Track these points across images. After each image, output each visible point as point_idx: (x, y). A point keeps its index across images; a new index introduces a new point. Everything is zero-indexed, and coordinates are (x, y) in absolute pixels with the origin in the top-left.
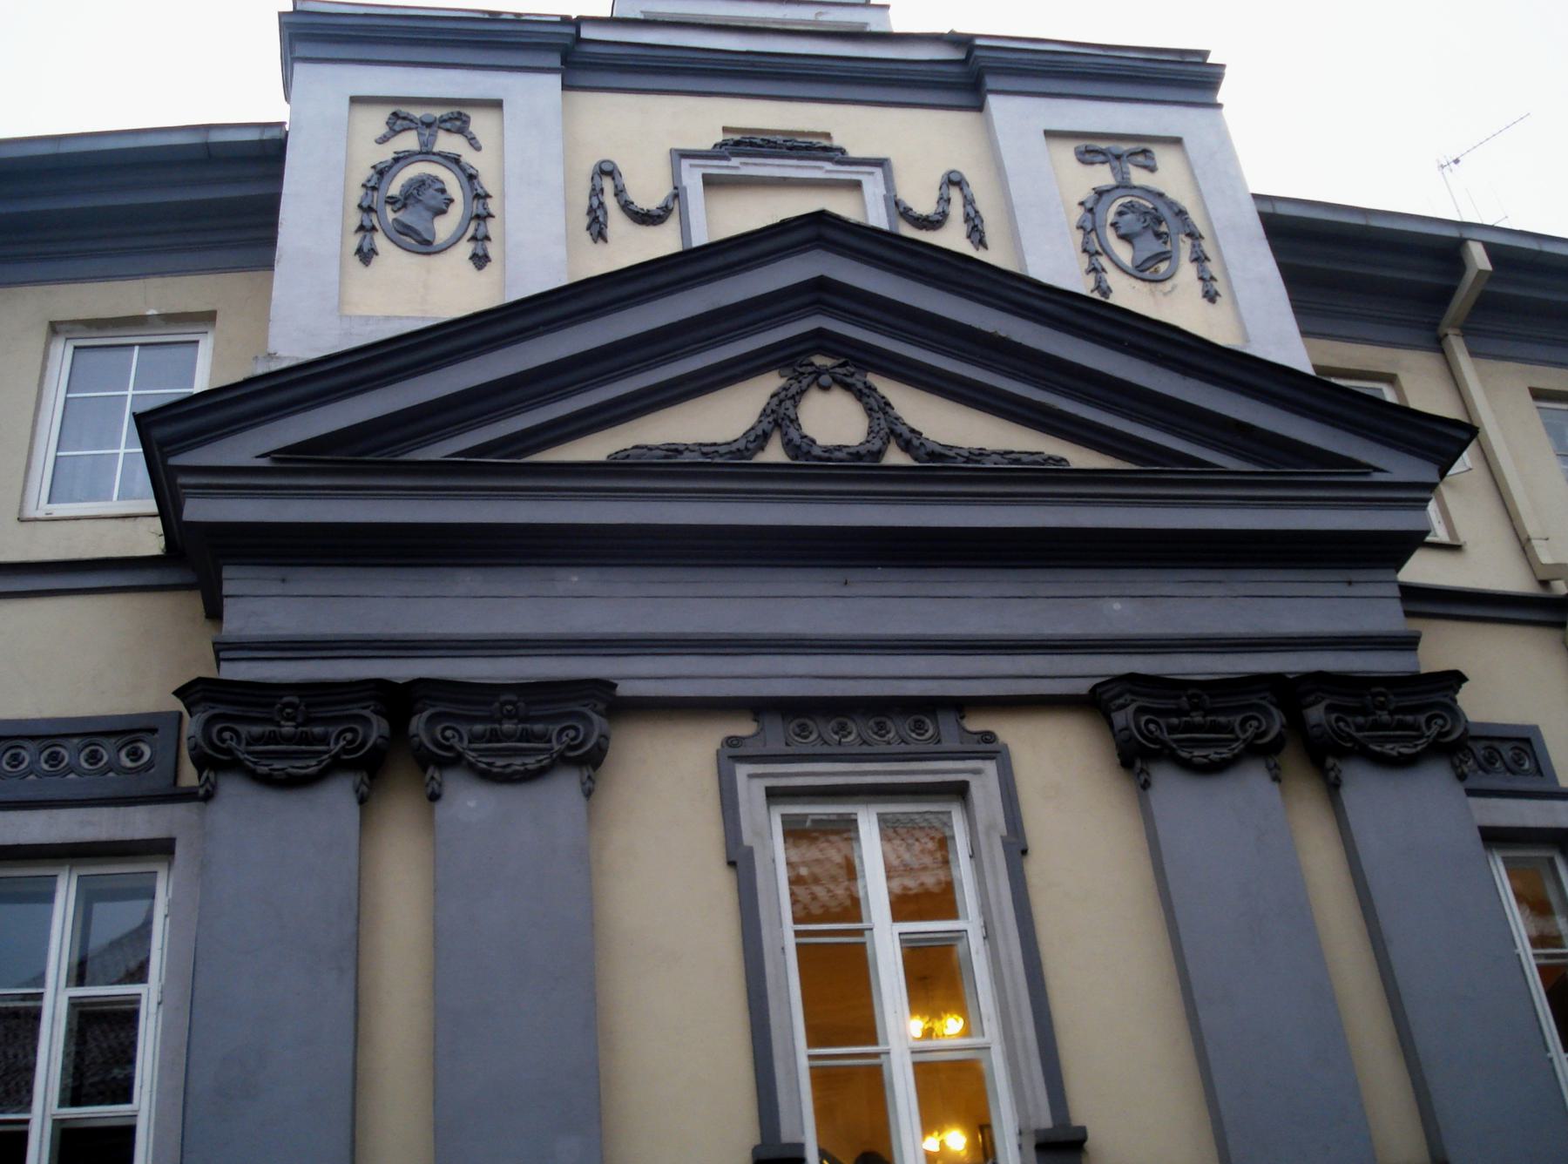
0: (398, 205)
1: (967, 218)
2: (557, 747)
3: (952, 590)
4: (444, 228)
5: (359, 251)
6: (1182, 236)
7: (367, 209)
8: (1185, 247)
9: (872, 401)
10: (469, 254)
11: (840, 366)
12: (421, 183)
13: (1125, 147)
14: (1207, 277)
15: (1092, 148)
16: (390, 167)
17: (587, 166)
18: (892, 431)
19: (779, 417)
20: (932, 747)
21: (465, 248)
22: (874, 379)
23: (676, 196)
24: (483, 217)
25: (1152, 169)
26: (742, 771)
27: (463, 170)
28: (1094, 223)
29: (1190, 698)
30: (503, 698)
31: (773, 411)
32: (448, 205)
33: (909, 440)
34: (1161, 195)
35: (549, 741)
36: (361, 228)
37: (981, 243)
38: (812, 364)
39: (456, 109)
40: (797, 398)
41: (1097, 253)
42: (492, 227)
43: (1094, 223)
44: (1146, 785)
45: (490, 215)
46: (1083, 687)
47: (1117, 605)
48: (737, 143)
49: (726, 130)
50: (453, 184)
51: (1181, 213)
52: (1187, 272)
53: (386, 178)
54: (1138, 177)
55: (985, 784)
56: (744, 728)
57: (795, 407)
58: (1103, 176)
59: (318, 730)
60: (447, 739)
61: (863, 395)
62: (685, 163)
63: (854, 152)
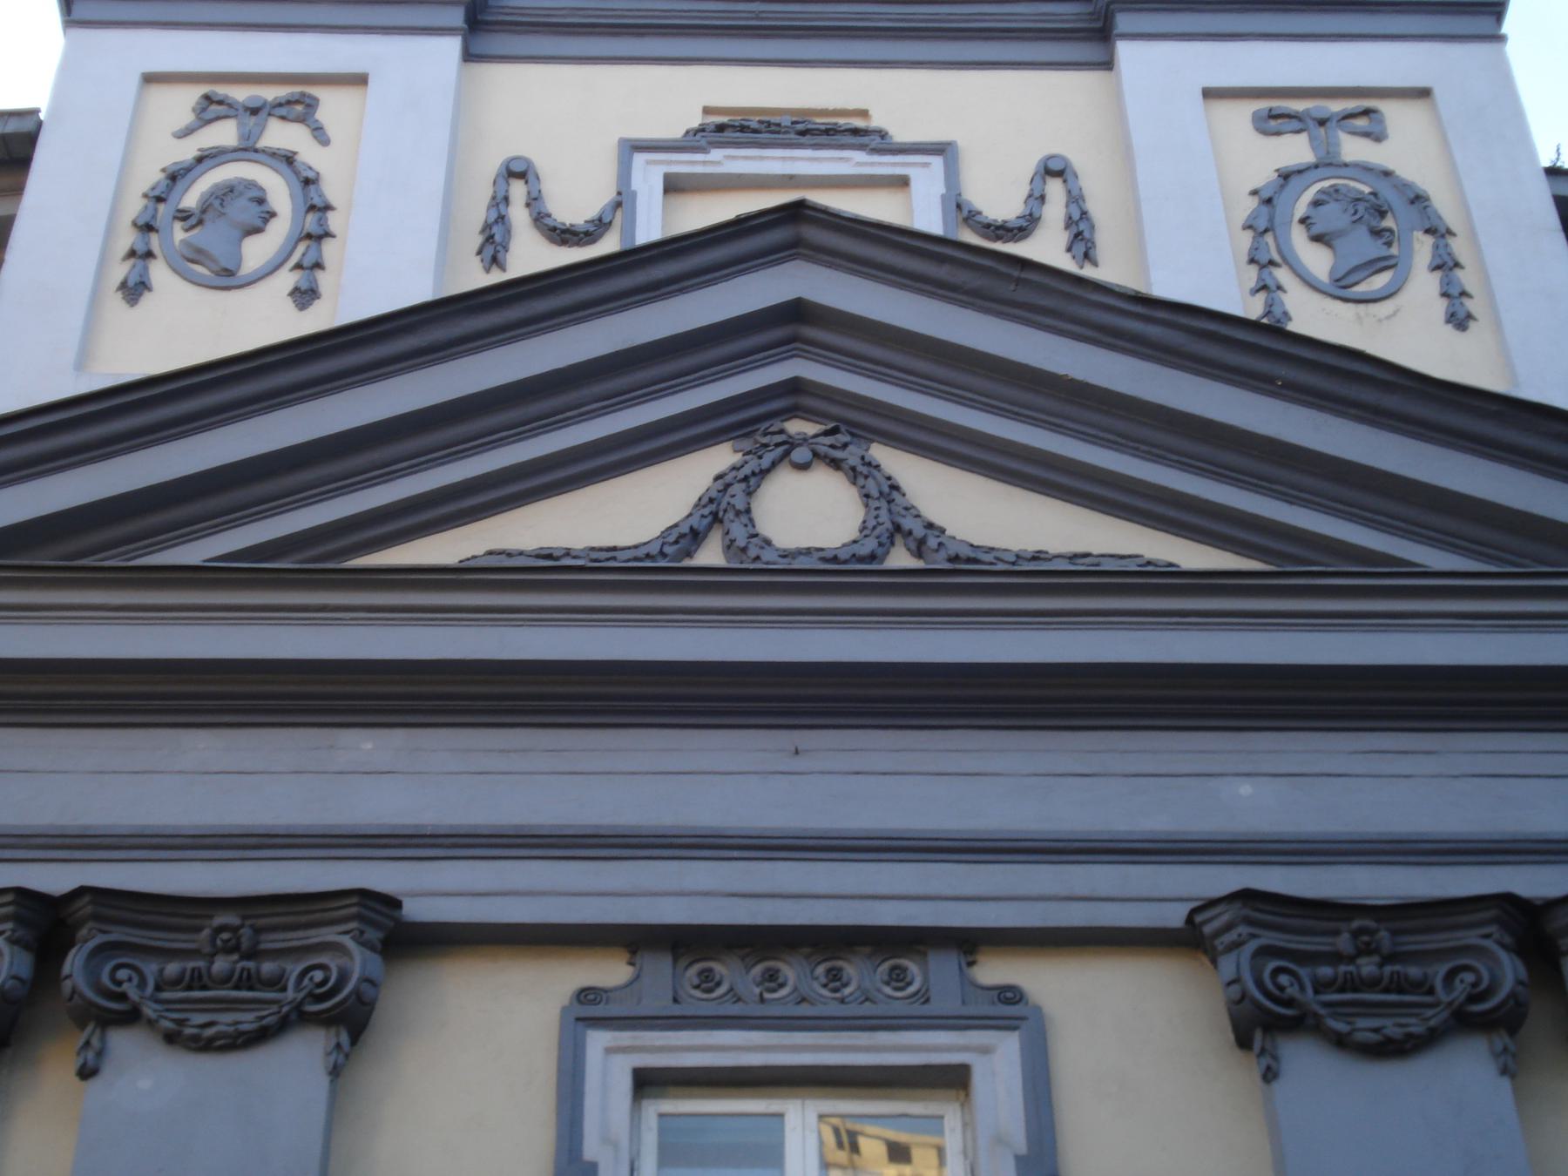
0: (193, 221)
1: (1069, 222)
2: (290, 994)
3: (970, 763)
4: (256, 252)
5: (123, 285)
6: (1419, 235)
7: (148, 228)
8: (1423, 248)
9: (870, 483)
10: (290, 287)
11: (826, 433)
12: (227, 192)
13: (1337, 106)
14: (1455, 292)
15: (1277, 112)
16: (188, 170)
17: (492, 165)
18: (898, 528)
19: (721, 509)
20: (918, 1009)
21: (287, 279)
22: (881, 454)
23: (618, 205)
24: (319, 237)
25: (1377, 136)
26: (598, 1040)
27: (297, 173)
28: (1271, 220)
29: (1356, 934)
30: (219, 920)
31: (711, 501)
32: (266, 221)
33: (925, 537)
34: (1387, 174)
35: (284, 989)
36: (132, 253)
37: (1088, 257)
38: (782, 432)
39: (297, 89)
40: (753, 480)
41: (1272, 263)
42: (329, 249)
43: (1271, 220)
44: (1270, 1075)
45: (328, 234)
46: (1174, 916)
47: (1245, 789)
48: (721, 128)
49: (707, 111)
50: (278, 190)
51: (1418, 199)
52: (1423, 286)
53: (180, 185)
54: (1354, 149)
55: (997, 1063)
56: (611, 971)
57: (750, 493)
58: (1296, 150)
59: (268, 967)
60: (119, 983)
61: (860, 474)
62: (639, 159)
63: (900, 135)
